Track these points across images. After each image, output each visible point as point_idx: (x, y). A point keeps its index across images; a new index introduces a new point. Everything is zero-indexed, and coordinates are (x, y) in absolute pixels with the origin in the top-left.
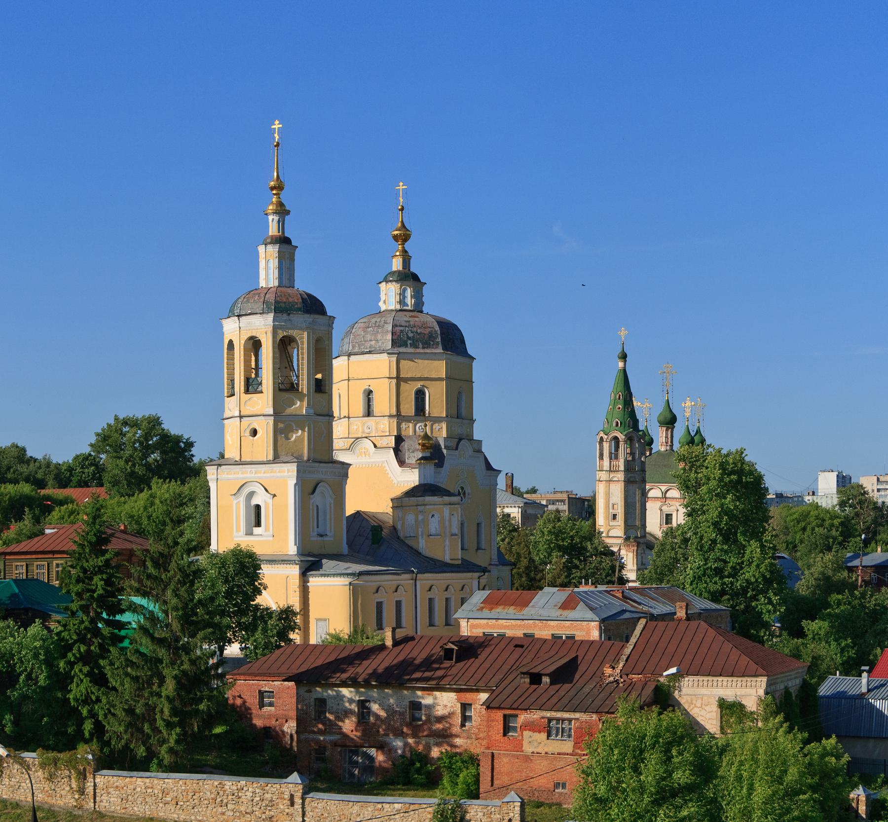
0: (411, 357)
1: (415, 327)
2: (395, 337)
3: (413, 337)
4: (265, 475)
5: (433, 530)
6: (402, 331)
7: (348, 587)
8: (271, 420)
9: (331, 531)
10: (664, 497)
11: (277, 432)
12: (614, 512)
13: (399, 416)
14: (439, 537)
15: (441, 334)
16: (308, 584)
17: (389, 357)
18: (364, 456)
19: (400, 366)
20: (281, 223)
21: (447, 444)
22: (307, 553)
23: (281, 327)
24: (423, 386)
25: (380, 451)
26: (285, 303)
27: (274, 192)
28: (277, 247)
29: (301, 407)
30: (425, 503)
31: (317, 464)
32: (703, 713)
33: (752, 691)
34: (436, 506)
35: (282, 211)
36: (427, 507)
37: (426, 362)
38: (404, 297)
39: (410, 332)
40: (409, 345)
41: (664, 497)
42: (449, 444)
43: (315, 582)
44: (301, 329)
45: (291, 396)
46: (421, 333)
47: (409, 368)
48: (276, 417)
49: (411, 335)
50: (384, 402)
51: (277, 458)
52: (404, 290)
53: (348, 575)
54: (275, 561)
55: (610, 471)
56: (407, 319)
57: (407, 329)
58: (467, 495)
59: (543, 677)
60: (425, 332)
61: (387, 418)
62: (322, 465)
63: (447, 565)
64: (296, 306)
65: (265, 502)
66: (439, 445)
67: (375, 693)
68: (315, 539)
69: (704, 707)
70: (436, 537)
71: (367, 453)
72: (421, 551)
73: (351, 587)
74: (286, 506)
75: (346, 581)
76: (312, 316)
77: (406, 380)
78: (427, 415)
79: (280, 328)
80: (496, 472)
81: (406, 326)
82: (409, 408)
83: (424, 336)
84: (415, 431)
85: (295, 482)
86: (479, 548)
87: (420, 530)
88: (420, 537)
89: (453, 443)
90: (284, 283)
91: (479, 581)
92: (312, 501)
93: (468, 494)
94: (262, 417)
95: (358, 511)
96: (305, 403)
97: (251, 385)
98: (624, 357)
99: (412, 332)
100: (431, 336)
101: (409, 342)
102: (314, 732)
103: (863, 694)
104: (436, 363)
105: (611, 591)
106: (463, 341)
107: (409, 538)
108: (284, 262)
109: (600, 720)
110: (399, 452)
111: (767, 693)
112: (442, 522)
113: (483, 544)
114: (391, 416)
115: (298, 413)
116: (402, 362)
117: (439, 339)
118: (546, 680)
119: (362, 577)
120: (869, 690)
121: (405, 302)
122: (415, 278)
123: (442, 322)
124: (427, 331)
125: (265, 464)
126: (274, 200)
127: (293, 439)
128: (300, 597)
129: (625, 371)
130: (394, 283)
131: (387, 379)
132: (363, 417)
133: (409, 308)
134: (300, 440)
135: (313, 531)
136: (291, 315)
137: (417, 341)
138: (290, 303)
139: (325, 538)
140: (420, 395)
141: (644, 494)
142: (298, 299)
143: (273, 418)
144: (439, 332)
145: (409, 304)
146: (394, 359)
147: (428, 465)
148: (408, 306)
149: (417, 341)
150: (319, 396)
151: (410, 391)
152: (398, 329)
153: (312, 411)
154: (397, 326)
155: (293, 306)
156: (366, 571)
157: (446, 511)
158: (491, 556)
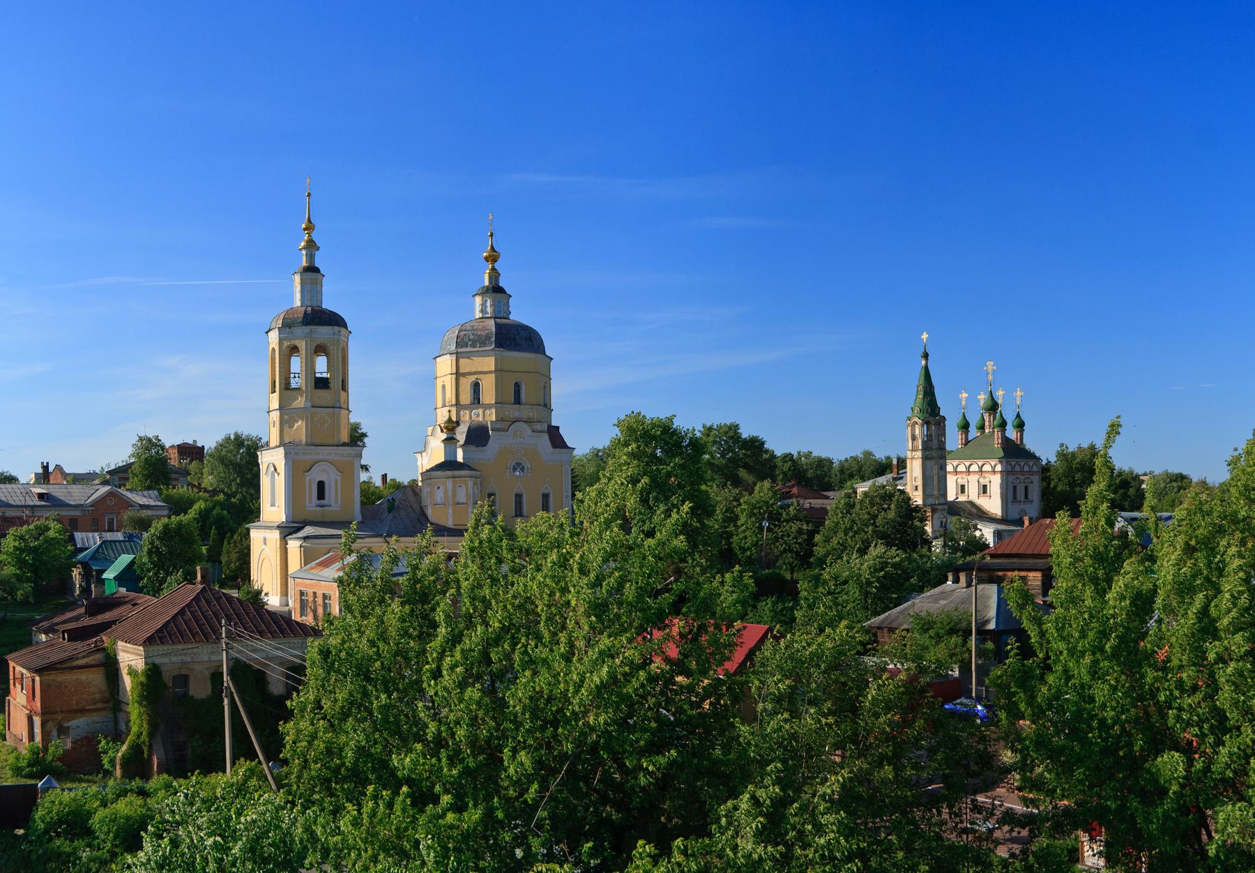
0: (468, 355)
5: (439, 501)
6: (465, 335)
10: (981, 471)
12: (915, 484)
15: (496, 333)
20: (311, 257)
21: (494, 426)
31: (315, 447)
35: (311, 246)
38: (486, 307)
41: (981, 471)
42: (499, 426)
44: (300, 338)
47: (467, 366)
50: (488, 396)
52: (486, 301)
55: (912, 450)
66: (488, 428)
77: (464, 375)
82: (466, 398)
84: (471, 417)
92: (307, 479)
96: (304, 399)
97: (274, 392)
98: (926, 356)
100: (488, 337)
104: (487, 359)
112: (446, 492)
116: (461, 360)
117: (493, 339)
126: (306, 238)
129: (926, 368)
133: (489, 315)
134: (299, 427)
140: (476, 387)
141: (943, 468)
146: (454, 357)
151: (466, 383)
152: (462, 333)
153: (309, 404)
157: (450, 483)
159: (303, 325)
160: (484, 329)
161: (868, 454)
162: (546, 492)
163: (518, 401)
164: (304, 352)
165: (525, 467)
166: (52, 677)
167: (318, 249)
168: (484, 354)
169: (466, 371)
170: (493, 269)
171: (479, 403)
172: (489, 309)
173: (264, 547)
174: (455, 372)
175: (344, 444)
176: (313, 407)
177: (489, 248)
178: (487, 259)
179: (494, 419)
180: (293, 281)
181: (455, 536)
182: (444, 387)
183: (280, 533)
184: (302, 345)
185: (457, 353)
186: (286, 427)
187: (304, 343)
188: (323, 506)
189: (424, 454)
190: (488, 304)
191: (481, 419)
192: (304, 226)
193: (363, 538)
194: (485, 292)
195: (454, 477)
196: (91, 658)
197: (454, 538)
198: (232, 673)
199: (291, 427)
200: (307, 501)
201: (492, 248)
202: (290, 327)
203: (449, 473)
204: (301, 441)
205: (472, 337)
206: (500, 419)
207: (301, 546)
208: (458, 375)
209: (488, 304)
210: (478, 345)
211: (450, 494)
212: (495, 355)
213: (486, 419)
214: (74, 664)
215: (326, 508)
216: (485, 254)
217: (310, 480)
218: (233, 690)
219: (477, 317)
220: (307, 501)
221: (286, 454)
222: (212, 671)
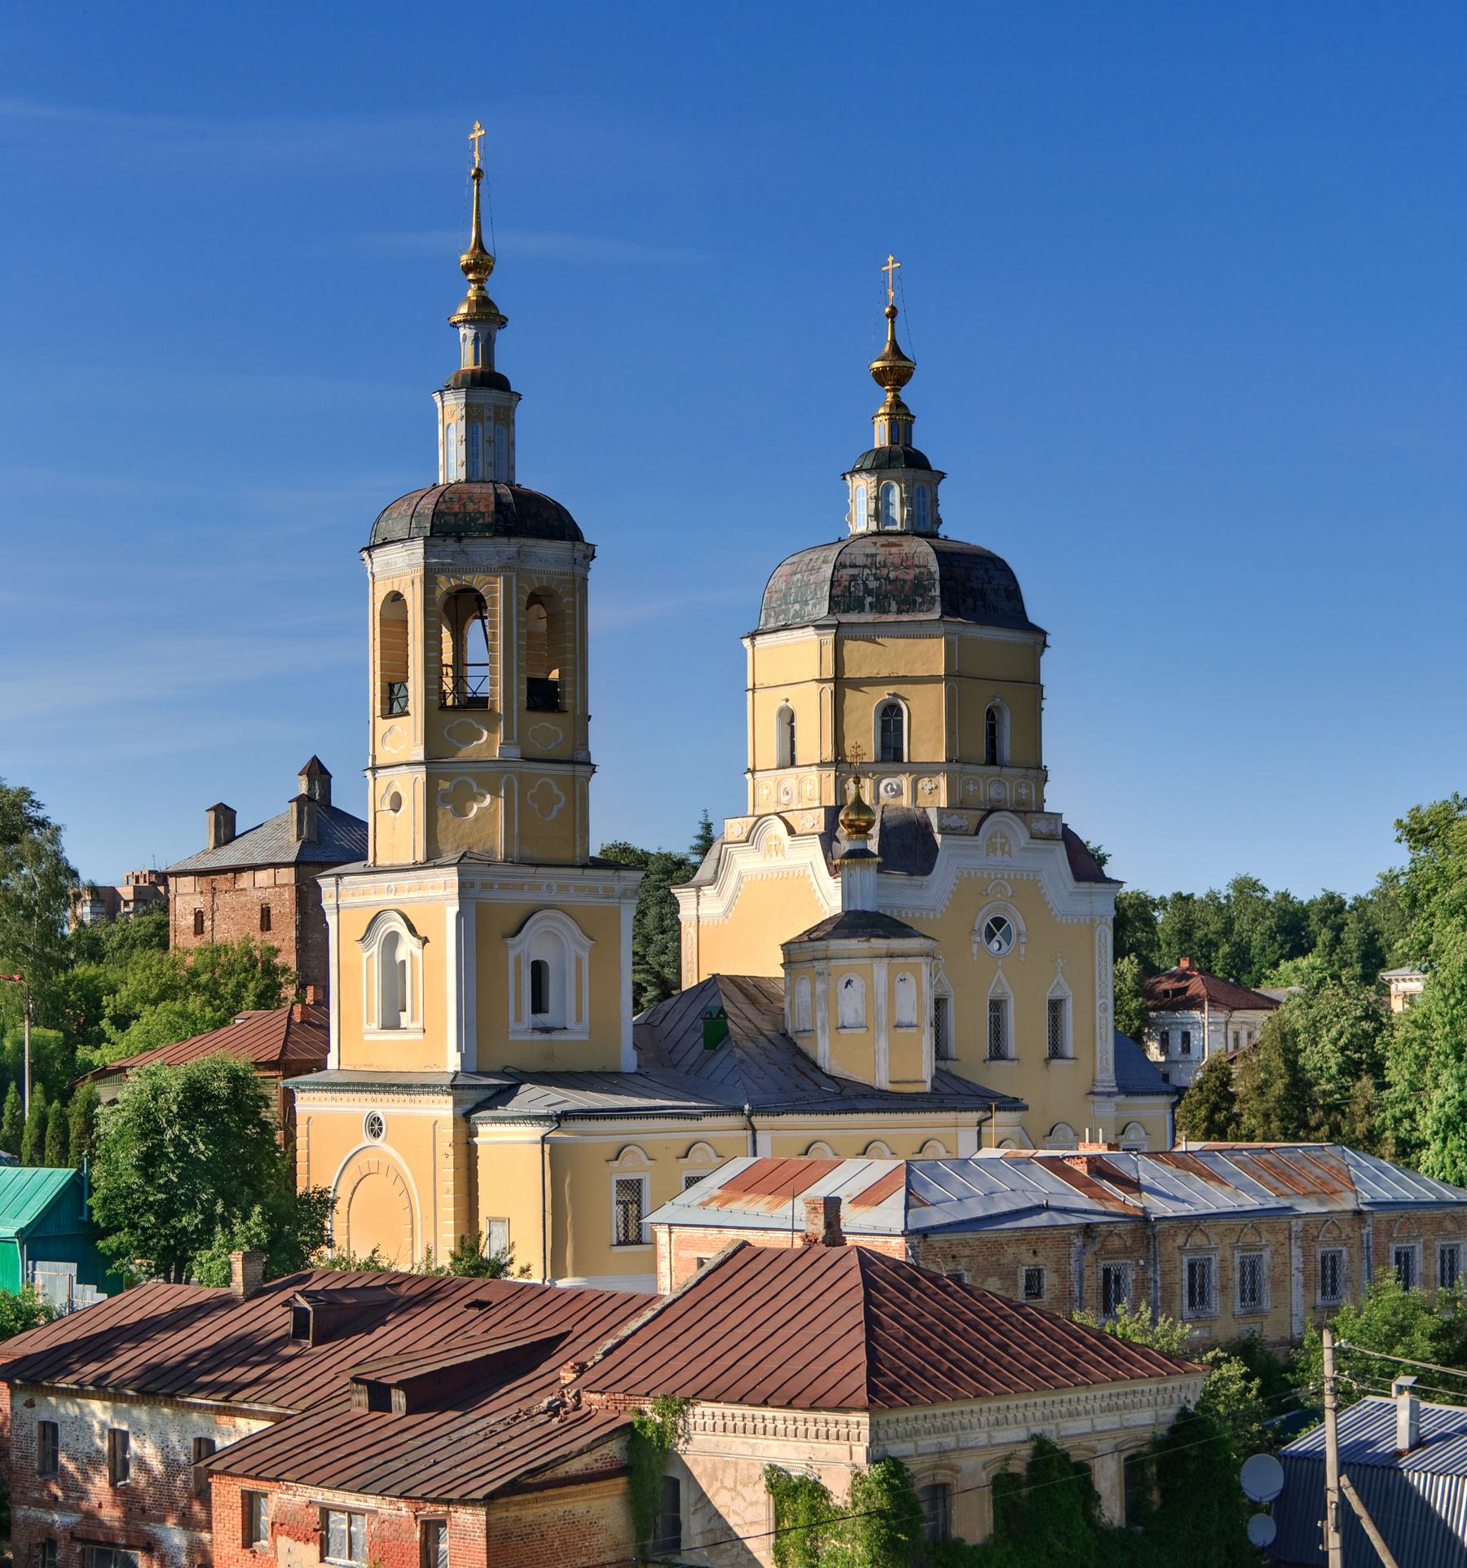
0: (868, 635)
1: (885, 566)
2: (837, 591)
3: (879, 588)
4: (413, 895)
6: (853, 578)
7: (540, 1146)
8: (421, 774)
9: (579, 1018)
11: (433, 800)
13: (840, 762)
14: (861, 1031)
16: (475, 1139)
17: (818, 635)
18: (774, 854)
19: (845, 653)
20: (485, 347)
21: (945, 822)
22: (498, 1068)
23: (443, 569)
24: (895, 695)
25: (799, 841)
26: (456, 515)
27: (471, 276)
28: (462, 394)
29: (490, 743)
30: (829, 954)
31: (531, 870)
32: (739, 1504)
33: (839, 1450)
34: (853, 961)
35: (487, 316)
36: (834, 962)
37: (902, 642)
38: (888, 505)
39: (871, 578)
40: (867, 606)
42: (954, 821)
43: (490, 1134)
44: (488, 571)
45: (469, 720)
46: (897, 579)
47: (862, 658)
48: (430, 766)
49: (873, 584)
51: (432, 858)
52: (888, 490)
53: (538, 1118)
54: (410, 1086)
56: (872, 550)
57: (867, 571)
58: (1014, 938)
59: (393, 1391)
60: (906, 577)
61: (814, 768)
62: (541, 870)
63: (883, 1095)
64: (481, 521)
65: (411, 955)
66: (928, 825)
67: (142, 1413)
68: (528, 1037)
69: (739, 1487)
70: (854, 1031)
71: (778, 849)
72: (820, 1063)
73: (547, 1147)
74: (444, 961)
75: (535, 1132)
76: (513, 540)
77: (858, 684)
78: (906, 759)
79: (442, 572)
80: (1113, 885)
81: (865, 566)
82: (864, 740)
83: (902, 586)
85: (457, 908)
86: (1056, 1053)
87: (819, 1015)
88: (819, 1032)
89: (968, 819)
90: (480, 473)
91: (979, 1133)
92: (512, 954)
93: (1019, 935)
94: (405, 767)
95: (714, 976)
96: (499, 737)
97: (393, 702)
99: (877, 579)
100: (920, 585)
101: (869, 599)
102: (38, 1504)
103: (1399, 1454)
105: (1064, 1158)
106: (1013, 593)
107: (801, 1035)
108: (480, 428)
109: (416, 1518)
110: (835, 843)
111: (873, 1460)
112: (869, 996)
113: (1069, 1047)
114: (822, 764)
115: (484, 756)
116: (850, 646)
117: (937, 592)
118: (399, 1398)
119: (568, 1125)
120: (1418, 1443)
121: (888, 515)
122: (917, 461)
123: (953, 554)
124: (911, 575)
125: (408, 870)
127: (472, 814)
128: (456, 1168)
130: (864, 475)
131: (815, 684)
132: (779, 768)
133: (898, 527)
135: (518, 1018)
136: (465, 541)
137: (886, 597)
138: (466, 514)
139: (555, 1036)
140: (890, 716)
142: (487, 506)
143: (423, 768)
144: (937, 576)
145: (898, 518)
146: (829, 637)
147: (858, 869)
148: (894, 522)
149: (886, 597)
150: (544, 722)
151: (864, 709)
152: (846, 573)
153: (515, 752)
154: (845, 567)
155: (474, 519)
156: (582, 1111)
157: (880, 970)
158: (1094, 1074)
159: (497, 533)
160: (906, 563)
161: (1246, 887)
162: (1058, 994)
163: (992, 758)
164: (500, 608)
165: (1014, 931)
166: (513, 1513)
167: (503, 322)
168: (918, 631)
169: (863, 674)
170: (898, 405)
171: (898, 758)
172: (897, 512)
173: (367, 1140)
174: (829, 673)
175: (415, 867)
176: (528, 760)
177: (887, 348)
178: (880, 377)
179: (943, 804)
180: (429, 421)
181: (884, 1111)
182: (788, 719)
183: (456, 1104)
184: (495, 590)
185: (838, 626)
186: (445, 814)
187: (500, 584)
188: (547, 1030)
189: (707, 891)
190: (896, 495)
191: (905, 801)
192: (465, 259)
193: (697, 1117)
194: (882, 464)
195: (891, 956)
196: (597, 1454)
197: (888, 1116)
198: (1343, 1467)
199: (461, 812)
200: (512, 1017)
201: (895, 349)
202: (459, 539)
203: (879, 944)
204: (492, 851)
205: (873, 584)
206: (957, 804)
207: (543, 1138)
208: (841, 683)
209: (896, 495)
210: (894, 607)
211: (882, 1000)
212: (946, 634)
213: (921, 802)
214: (562, 1471)
215: (555, 1036)
216: (878, 364)
217: (518, 960)
218: (1358, 1508)
219: (861, 528)
220: (512, 1017)
221: (462, 886)
222: (994, 1470)
